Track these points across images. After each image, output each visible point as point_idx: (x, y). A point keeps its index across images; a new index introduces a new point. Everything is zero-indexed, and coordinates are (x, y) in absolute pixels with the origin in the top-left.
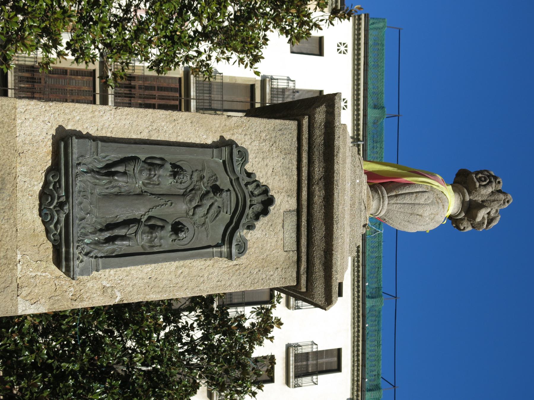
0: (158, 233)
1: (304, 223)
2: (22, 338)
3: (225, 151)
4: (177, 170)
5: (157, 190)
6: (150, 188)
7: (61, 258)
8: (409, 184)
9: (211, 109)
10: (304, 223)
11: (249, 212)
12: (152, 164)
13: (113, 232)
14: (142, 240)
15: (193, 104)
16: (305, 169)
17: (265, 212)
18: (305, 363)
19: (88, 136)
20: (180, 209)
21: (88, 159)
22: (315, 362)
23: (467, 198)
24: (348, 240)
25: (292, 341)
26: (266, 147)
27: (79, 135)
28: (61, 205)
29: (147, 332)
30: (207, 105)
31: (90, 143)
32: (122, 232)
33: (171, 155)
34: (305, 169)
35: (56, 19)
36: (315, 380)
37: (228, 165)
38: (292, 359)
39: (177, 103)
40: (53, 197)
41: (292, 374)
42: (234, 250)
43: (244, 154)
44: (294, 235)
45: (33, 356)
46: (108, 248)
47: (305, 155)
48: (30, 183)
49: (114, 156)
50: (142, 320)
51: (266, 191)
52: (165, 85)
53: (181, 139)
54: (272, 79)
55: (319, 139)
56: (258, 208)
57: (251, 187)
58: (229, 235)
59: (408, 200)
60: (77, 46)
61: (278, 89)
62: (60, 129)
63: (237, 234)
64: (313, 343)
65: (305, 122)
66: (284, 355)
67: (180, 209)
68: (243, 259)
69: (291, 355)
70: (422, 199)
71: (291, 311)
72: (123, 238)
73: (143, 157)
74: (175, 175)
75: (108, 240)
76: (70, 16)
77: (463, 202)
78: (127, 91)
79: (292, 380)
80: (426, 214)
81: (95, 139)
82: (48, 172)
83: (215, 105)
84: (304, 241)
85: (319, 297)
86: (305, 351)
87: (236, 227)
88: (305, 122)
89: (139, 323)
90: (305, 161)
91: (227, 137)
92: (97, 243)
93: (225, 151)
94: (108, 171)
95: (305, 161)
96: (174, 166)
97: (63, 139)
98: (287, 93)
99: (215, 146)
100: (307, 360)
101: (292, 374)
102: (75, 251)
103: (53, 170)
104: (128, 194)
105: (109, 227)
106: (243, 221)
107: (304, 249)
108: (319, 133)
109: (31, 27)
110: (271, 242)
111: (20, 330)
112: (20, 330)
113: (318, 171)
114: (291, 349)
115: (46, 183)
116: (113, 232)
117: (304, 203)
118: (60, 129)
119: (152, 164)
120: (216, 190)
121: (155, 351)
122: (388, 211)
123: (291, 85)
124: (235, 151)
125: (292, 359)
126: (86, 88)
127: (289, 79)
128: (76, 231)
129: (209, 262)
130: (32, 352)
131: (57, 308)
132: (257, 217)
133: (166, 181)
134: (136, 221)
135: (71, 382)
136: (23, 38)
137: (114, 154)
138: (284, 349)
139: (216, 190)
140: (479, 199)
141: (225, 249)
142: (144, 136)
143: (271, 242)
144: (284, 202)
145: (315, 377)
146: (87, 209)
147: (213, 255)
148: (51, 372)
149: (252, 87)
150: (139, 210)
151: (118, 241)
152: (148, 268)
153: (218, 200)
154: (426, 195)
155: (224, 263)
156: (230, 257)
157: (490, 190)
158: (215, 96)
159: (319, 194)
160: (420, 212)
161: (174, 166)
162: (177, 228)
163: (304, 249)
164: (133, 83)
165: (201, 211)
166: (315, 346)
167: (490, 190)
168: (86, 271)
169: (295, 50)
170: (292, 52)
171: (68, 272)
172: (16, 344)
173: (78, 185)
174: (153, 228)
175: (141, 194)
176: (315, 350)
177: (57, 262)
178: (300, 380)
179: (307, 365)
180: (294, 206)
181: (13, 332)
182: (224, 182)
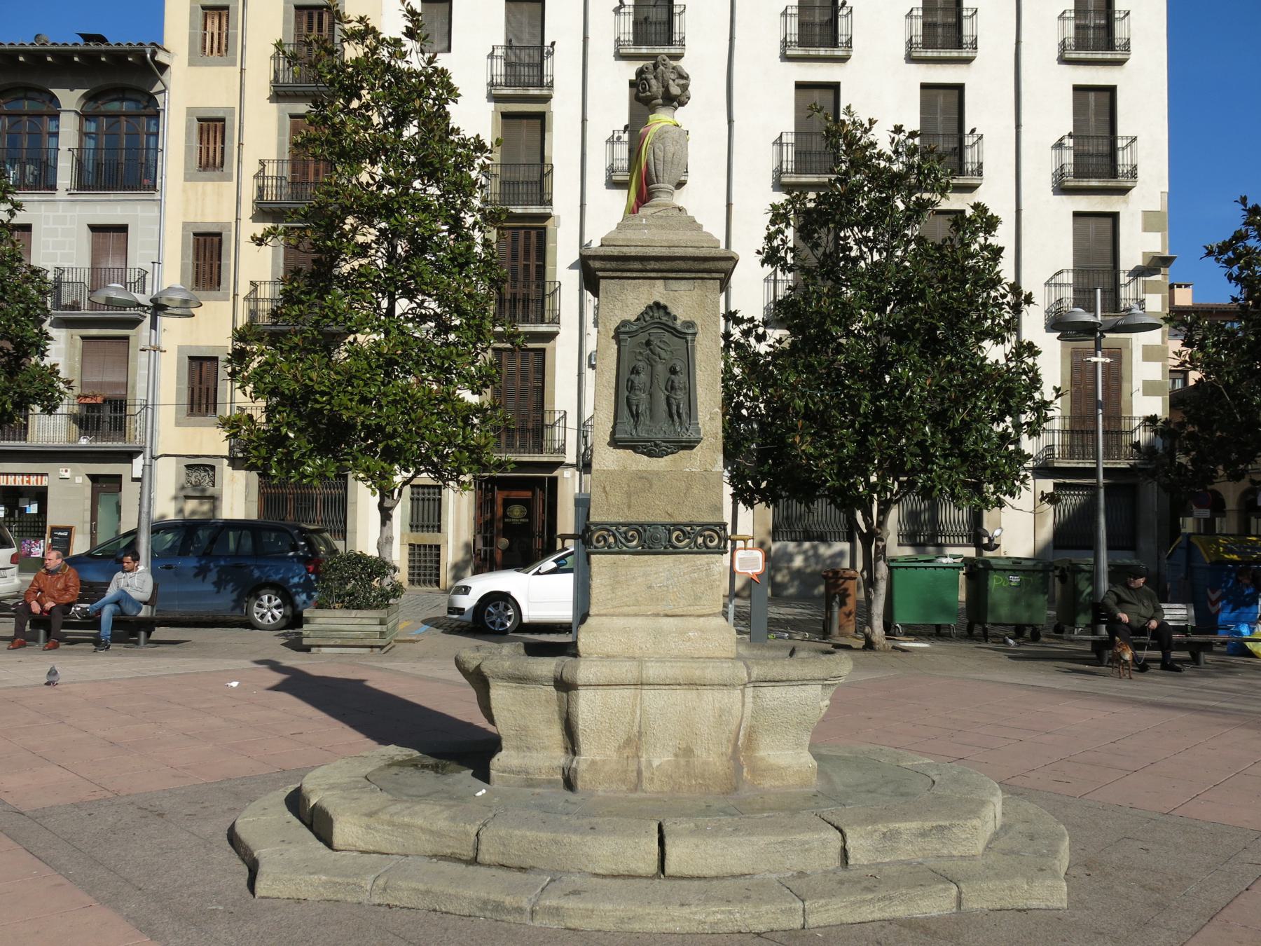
0: (676, 384)
1: (673, 275)
2: (826, 456)
3: (622, 336)
4: (635, 371)
5: (648, 384)
6: (647, 389)
7: (690, 445)
8: (647, 164)
9: (541, 182)
10: (673, 275)
11: (664, 319)
12: (631, 388)
13: (673, 414)
14: (680, 395)
15: (534, 210)
16: (635, 275)
17: (665, 308)
18: (940, 30)
19: (614, 427)
20: (661, 369)
21: (628, 428)
22: (940, 13)
23: (660, 101)
24: (689, 233)
25: (902, 52)
26: (619, 305)
27: (613, 434)
28: (656, 445)
29: (836, 307)
30: (535, 189)
31: (618, 427)
32: (674, 408)
33: (625, 374)
34: (635, 275)
35: (454, 409)
36: (970, 13)
37: (632, 334)
38: (930, 53)
39: (533, 233)
40: (653, 450)
41: (954, 54)
42: (690, 331)
43: (625, 323)
44: (683, 282)
45: (847, 444)
46: (684, 416)
47: (625, 274)
48: (642, 462)
49: (626, 412)
50: (821, 313)
51: (650, 307)
52: (508, 251)
53: (615, 367)
54: (492, 84)
55: (614, 265)
56: (662, 312)
57: (648, 318)
58: (680, 335)
59: (660, 167)
60: (479, 383)
61: (506, 75)
62: (609, 444)
63: (679, 328)
64: (909, 15)
65: (600, 274)
66: (923, 67)
67: (661, 369)
68: (698, 322)
69: (923, 54)
70: (660, 154)
71: (854, 54)
72: (678, 407)
73: (626, 393)
74: (638, 373)
75: (679, 416)
76: (449, 394)
77: (664, 105)
78: (520, 306)
79: (964, 54)
80: (672, 150)
81: (615, 424)
82: (636, 452)
83: (536, 177)
84: (687, 275)
85: (731, 263)
86: (920, 32)
87: (675, 329)
88: (600, 274)
89: (824, 317)
90: (629, 274)
91: (612, 334)
92: (681, 424)
93: (622, 336)
94: (636, 416)
95: (629, 274)
96: (632, 373)
97: (615, 443)
98: (513, 59)
99: (618, 342)
100: (935, 25)
101: (954, 54)
102: (685, 437)
103: (635, 449)
104: (651, 403)
105: (671, 416)
106: (670, 323)
107: (693, 275)
108: (608, 265)
109: (465, 438)
110: (684, 300)
111: (816, 458)
112: (815, 458)
113: (637, 265)
114: (915, 54)
115: (643, 453)
116: (673, 414)
117: (659, 275)
118: (609, 444)
119: (631, 388)
120: (648, 343)
121: (862, 297)
122: (669, 183)
123: (499, 52)
124: (622, 330)
125: (930, 53)
126: (519, 361)
127: (491, 56)
128: (673, 437)
129: (698, 348)
130: (843, 446)
131: (720, 448)
132: (668, 314)
133: (643, 377)
134: (668, 398)
135: (884, 403)
136: (479, 447)
137: (625, 411)
138: (913, 66)
139: (648, 343)
140: (661, 90)
141: (689, 338)
142: (613, 391)
143: (684, 300)
144: (657, 291)
145: (965, 13)
146: (661, 430)
147: (693, 347)
148: (870, 424)
149: (505, 116)
150: (661, 397)
151: (680, 409)
152: (700, 390)
153: (656, 342)
154: (657, 151)
155: (699, 338)
156: (695, 334)
157: (653, 82)
158: (522, 174)
159: (652, 265)
160: (670, 155)
161: (632, 373)
162: (673, 371)
163: (693, 275)
164: (508, 297)
165: (663, 354)
166: (915, 13)
167: (653, 82)
168: (698, 431)
169: (445, 45)
170: (449, 50)
171: (698, 442)
172: (833, 462)
173: (644, 435)
174: (672, 388)
175: (651, 395)
176: (920, 13)
177: (693, 447)
178: (967, 40)
179: (944, 25)
180: (662, 281)
181: (817, 466)
182: (642, 338)
